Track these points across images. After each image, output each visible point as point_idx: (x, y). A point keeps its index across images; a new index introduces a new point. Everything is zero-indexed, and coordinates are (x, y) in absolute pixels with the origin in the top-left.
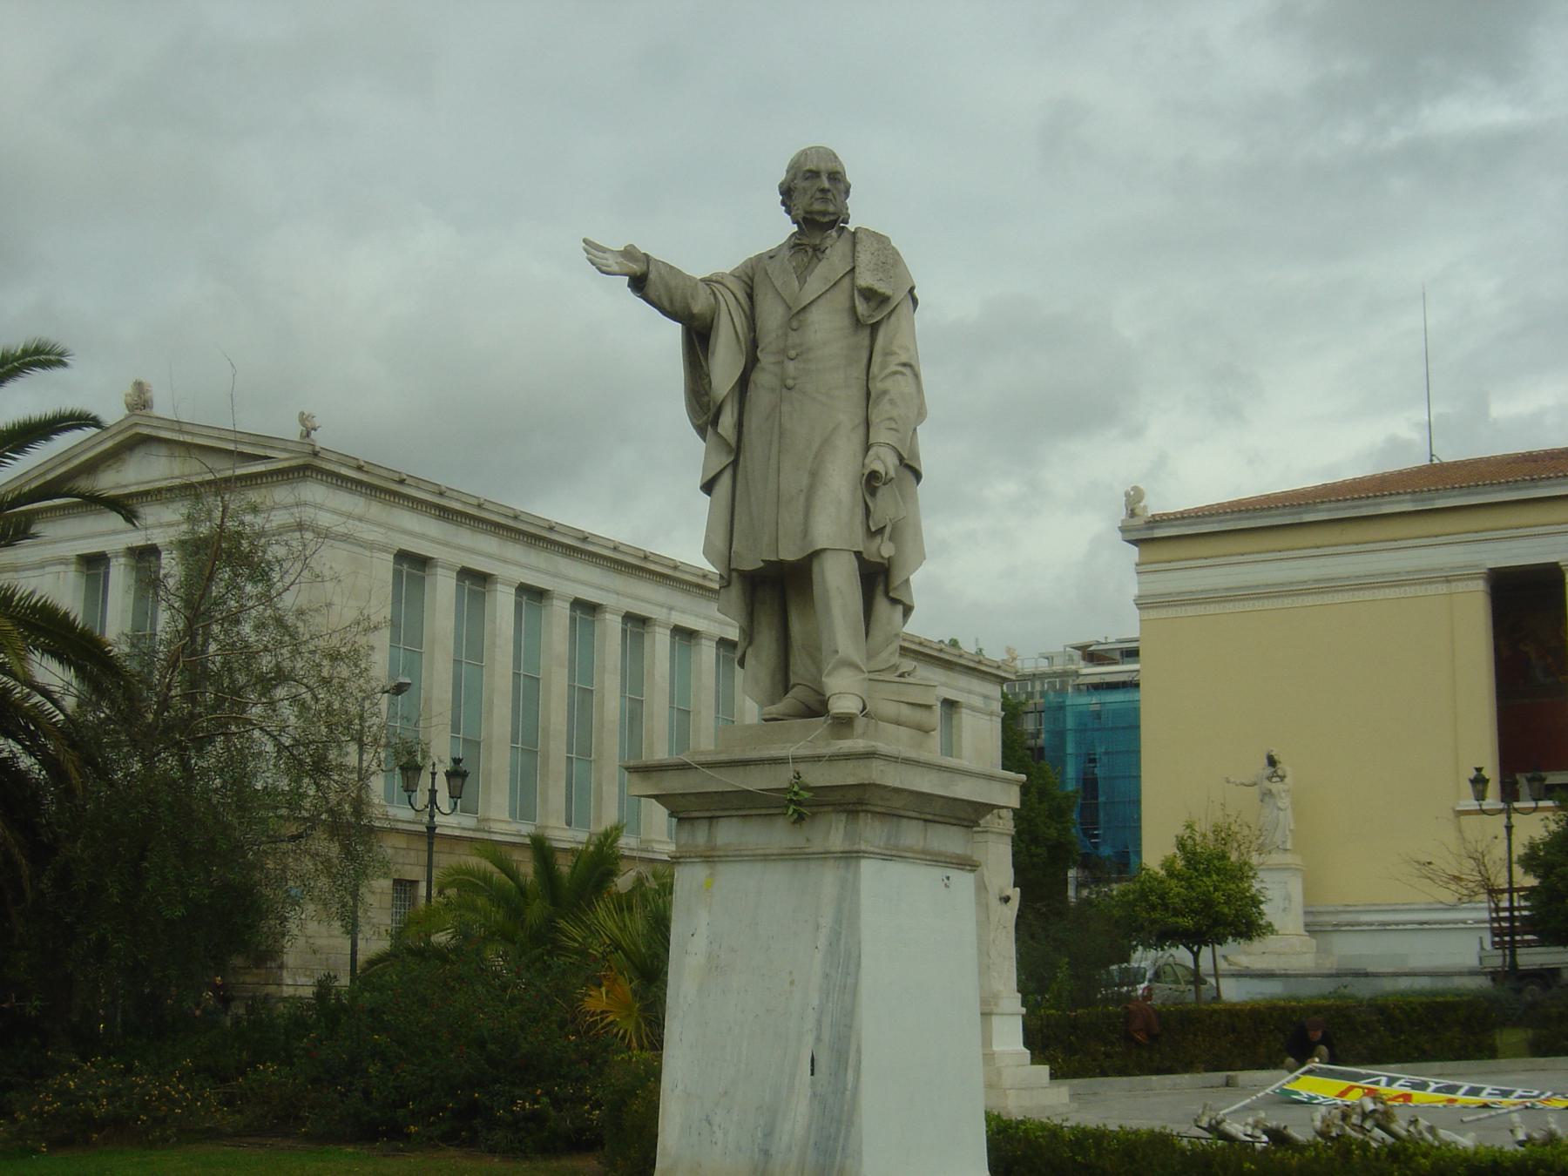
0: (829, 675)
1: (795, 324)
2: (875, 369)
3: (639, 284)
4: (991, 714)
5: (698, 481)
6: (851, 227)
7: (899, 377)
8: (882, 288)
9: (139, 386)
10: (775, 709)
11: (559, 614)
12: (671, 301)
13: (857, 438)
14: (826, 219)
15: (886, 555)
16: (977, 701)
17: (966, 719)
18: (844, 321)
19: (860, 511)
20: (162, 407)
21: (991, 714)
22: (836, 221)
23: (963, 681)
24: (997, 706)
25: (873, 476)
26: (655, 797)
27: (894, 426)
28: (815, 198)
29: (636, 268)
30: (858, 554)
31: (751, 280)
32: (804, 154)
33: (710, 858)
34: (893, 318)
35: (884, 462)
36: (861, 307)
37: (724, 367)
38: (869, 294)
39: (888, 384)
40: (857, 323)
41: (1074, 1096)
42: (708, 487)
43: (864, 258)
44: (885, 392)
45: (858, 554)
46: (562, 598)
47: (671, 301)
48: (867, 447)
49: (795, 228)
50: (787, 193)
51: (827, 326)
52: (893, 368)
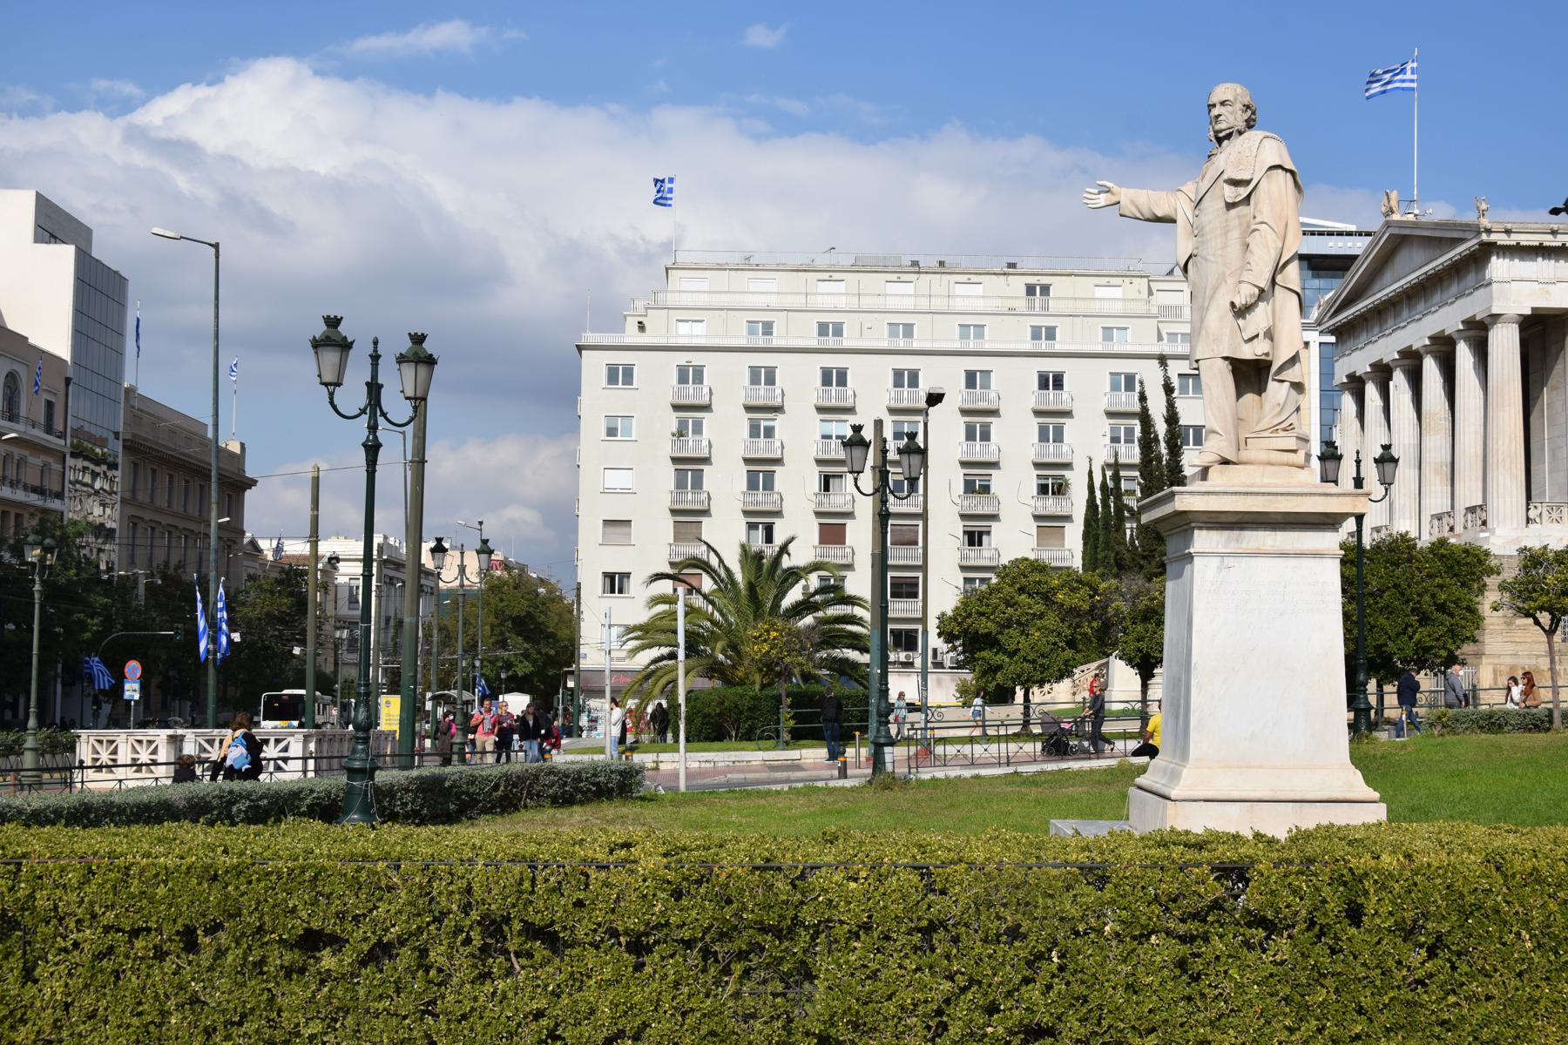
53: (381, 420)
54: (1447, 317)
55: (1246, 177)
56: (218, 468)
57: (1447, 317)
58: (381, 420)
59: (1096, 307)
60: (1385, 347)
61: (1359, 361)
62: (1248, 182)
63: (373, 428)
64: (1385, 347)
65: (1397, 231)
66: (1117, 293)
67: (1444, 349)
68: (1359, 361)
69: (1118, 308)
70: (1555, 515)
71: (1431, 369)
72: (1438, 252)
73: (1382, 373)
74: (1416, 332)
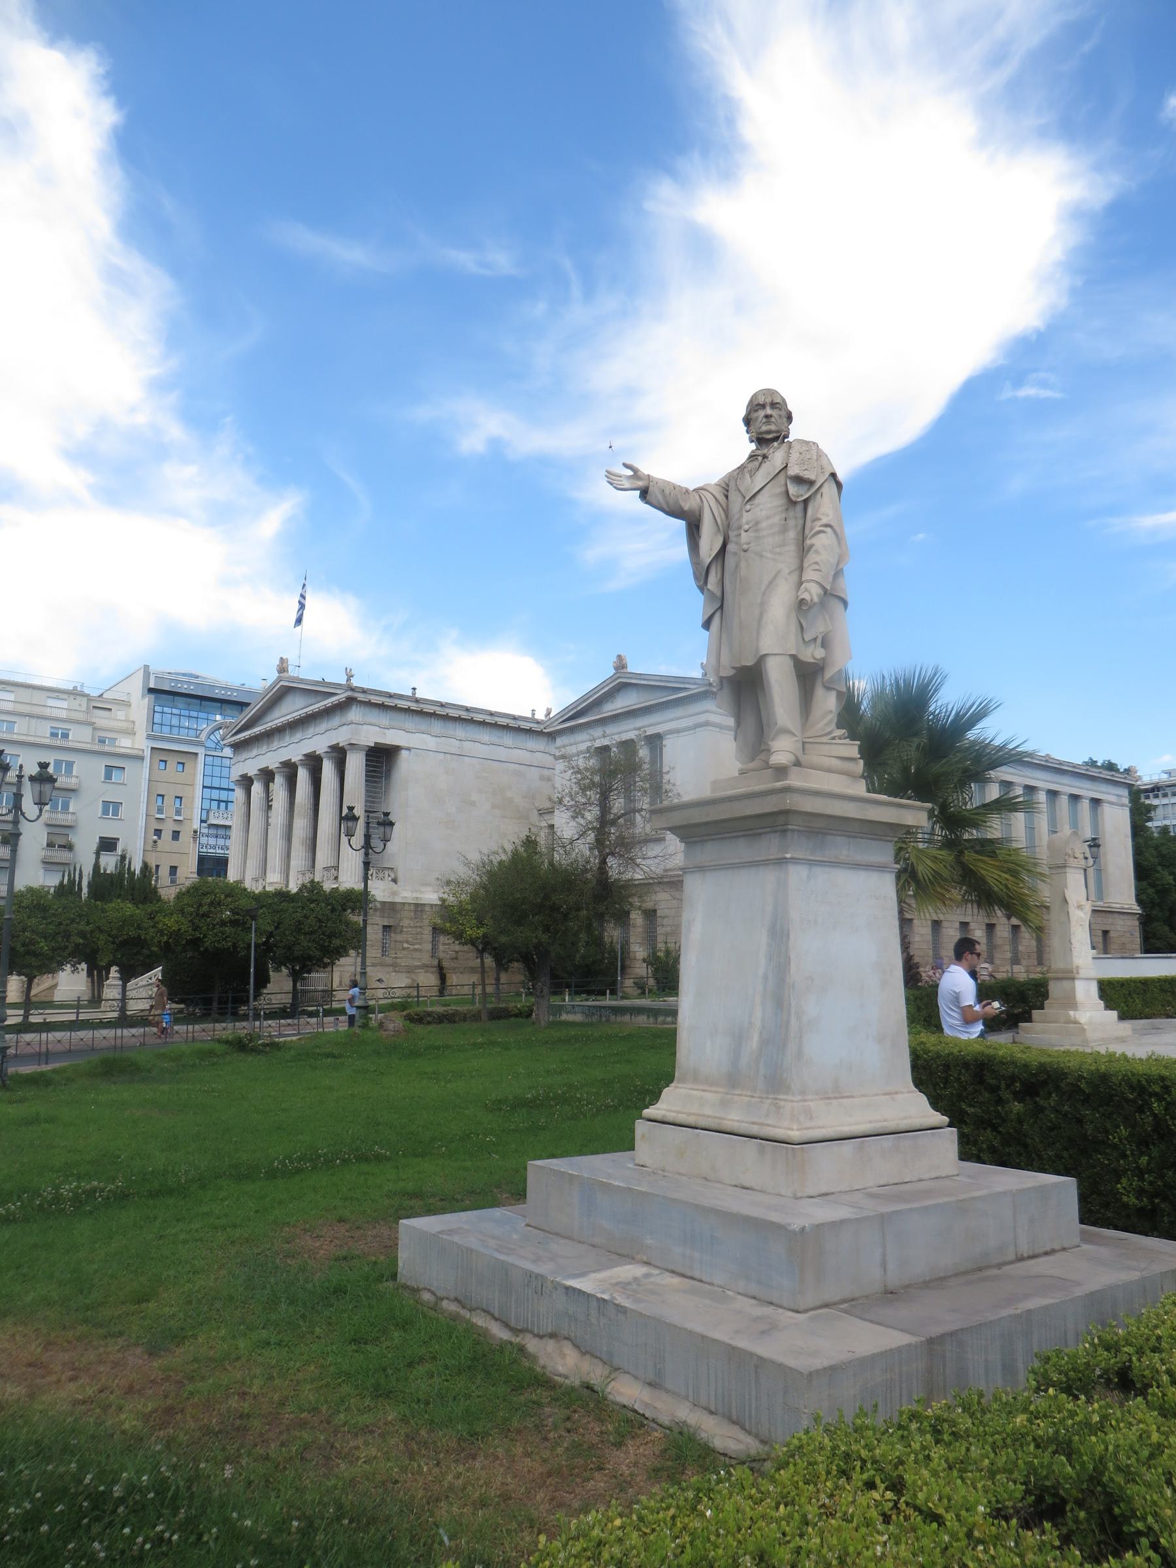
0: (773, 739)
1: (748, 507)
2: (807, 531)
3: (644, 494)
4: (1123, 805)
5: (700, 619)
6: (791, 439)
7: (822, 535)
8: (807, 475)
9: (619, 656)
10: (752, 765)
11: (1064, 800)
12: (667, 503)
13: (794, 578)
14: (770, 436)
15: (818, 657)
16: (1113, 799)
17: (1107, 810)
18: (780, 501)
19: (794, 627)
20: (632, 668)
21: (1123, 805)
22: (780, 437)
23: (1104, 787)
24: (1126, 801)
25: (802, 602)
26: (670, 829)
27: (817, 567)
28: (767, 420)
29: (640, 484)
30: (794, 657)
31: (727, 487)
32: (755, 396)
33: (701, 869)
34: (819, 496)
35: (812, 592)
36: (793, 489)
37: (709, 544)
38: (799, 480)
39: (815, 541)
40: (792, 503)
41: (1134, 1030)
42: (707, 625)
43: (794, 456)
44: (812, 546)
45: (794, 657)
46: (1065, 794)
47: (667, 503)
48: (800, 583)
49: (753, 446)
50: (748, 421)
51: (768, 506)
52: (818, 529)
53: (21, 817)
54: (318, 740)
55: (813, 477)
56: (1156, 807)
57: (318, 740)
58: (21, 817)
59: (47, 712)
60: (270, 757)
61: (252, 763)
62: (811, 483)
63: (367, 854)
64: (270, 757)
65: (286, 684)
66: (65, 705)
67: (314, 763)
68: (252, 763)
69: (63, 714)
70: (381, 875)
71: (303, 775)
72: (313, 701)
73: (267, 776)
74: (294, 749)
